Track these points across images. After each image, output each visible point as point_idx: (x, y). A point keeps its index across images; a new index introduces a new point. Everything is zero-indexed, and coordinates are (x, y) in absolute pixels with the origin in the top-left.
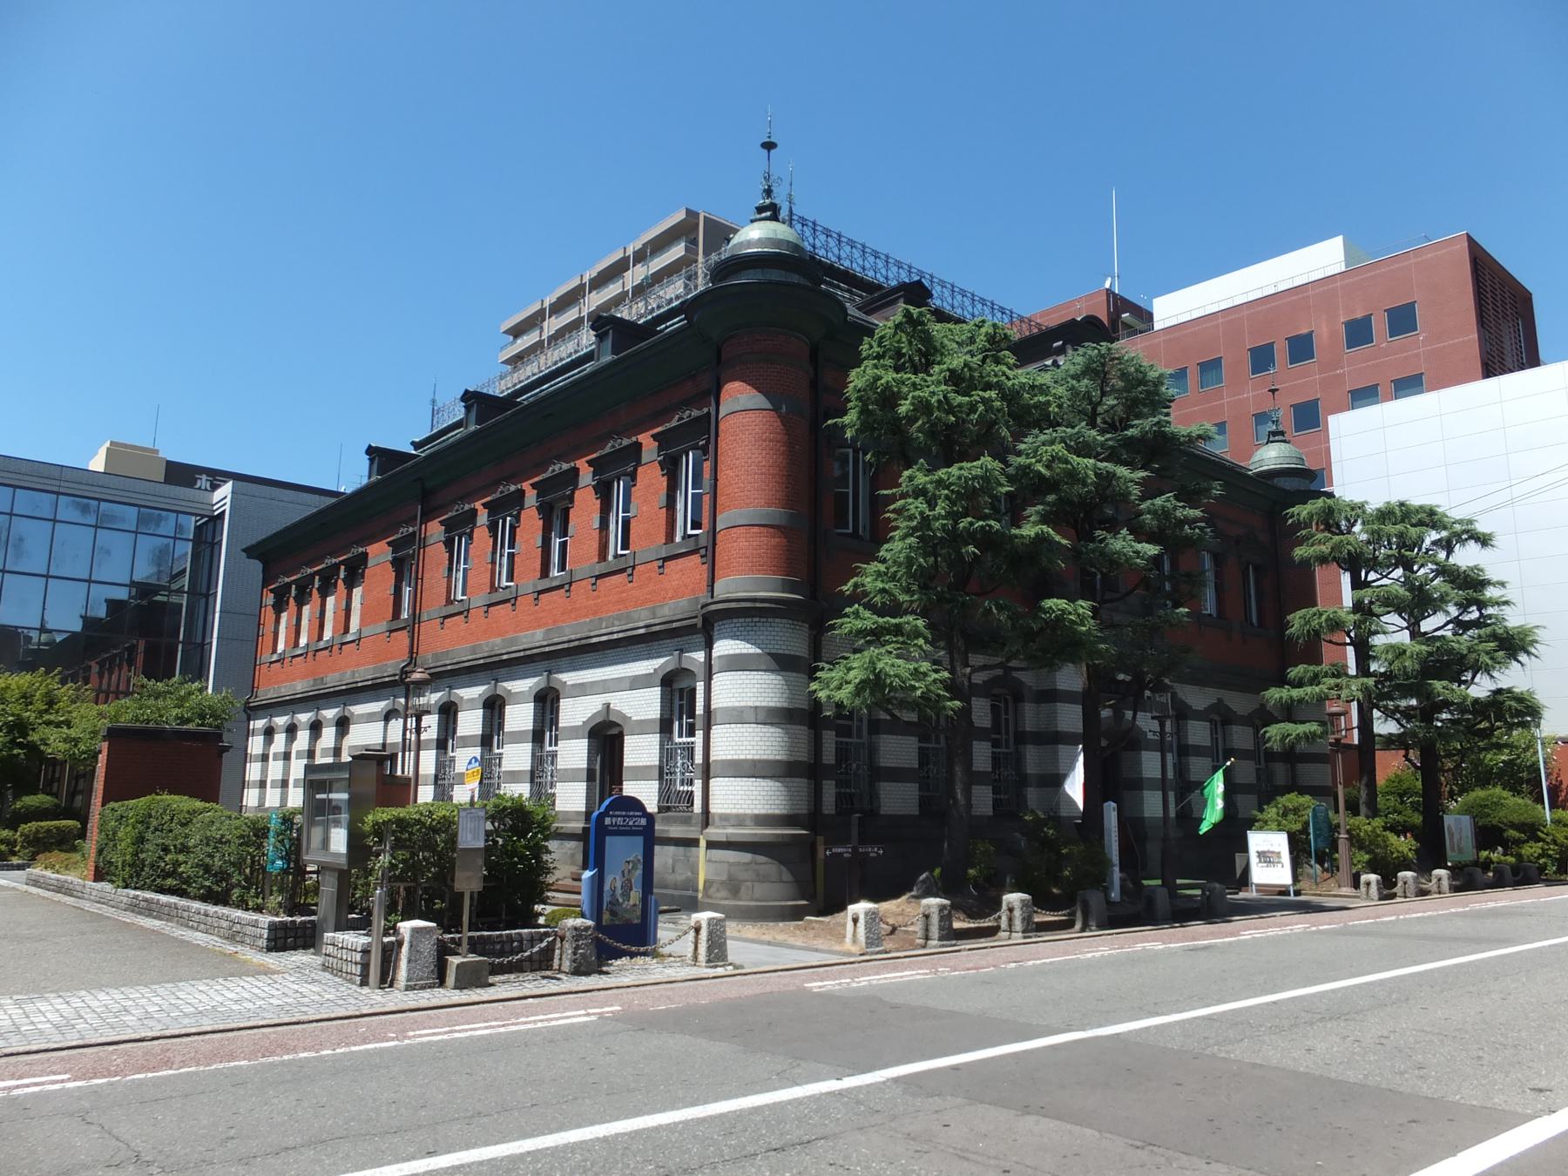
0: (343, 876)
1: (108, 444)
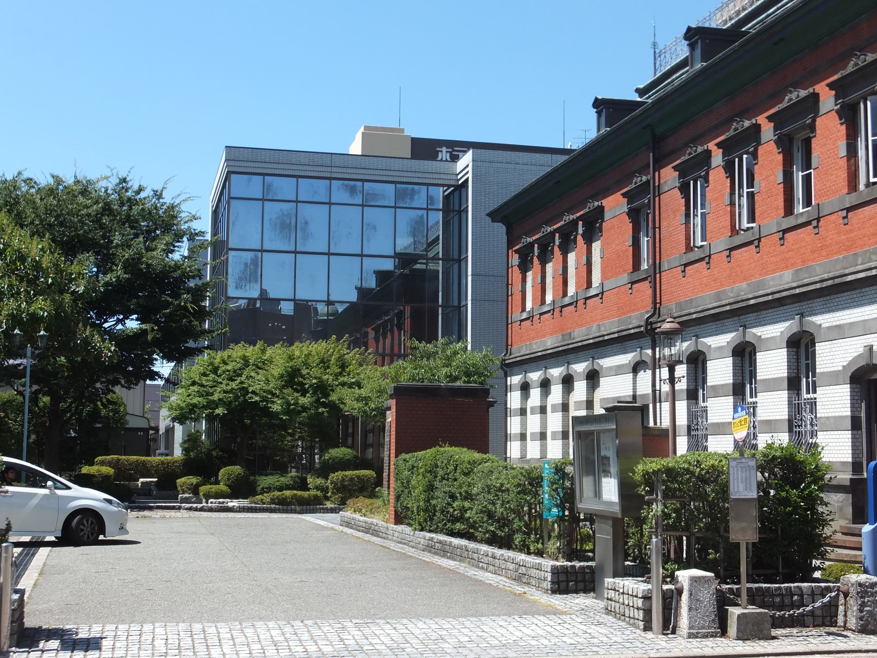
0: (617, 523)
1: (362, 129)
